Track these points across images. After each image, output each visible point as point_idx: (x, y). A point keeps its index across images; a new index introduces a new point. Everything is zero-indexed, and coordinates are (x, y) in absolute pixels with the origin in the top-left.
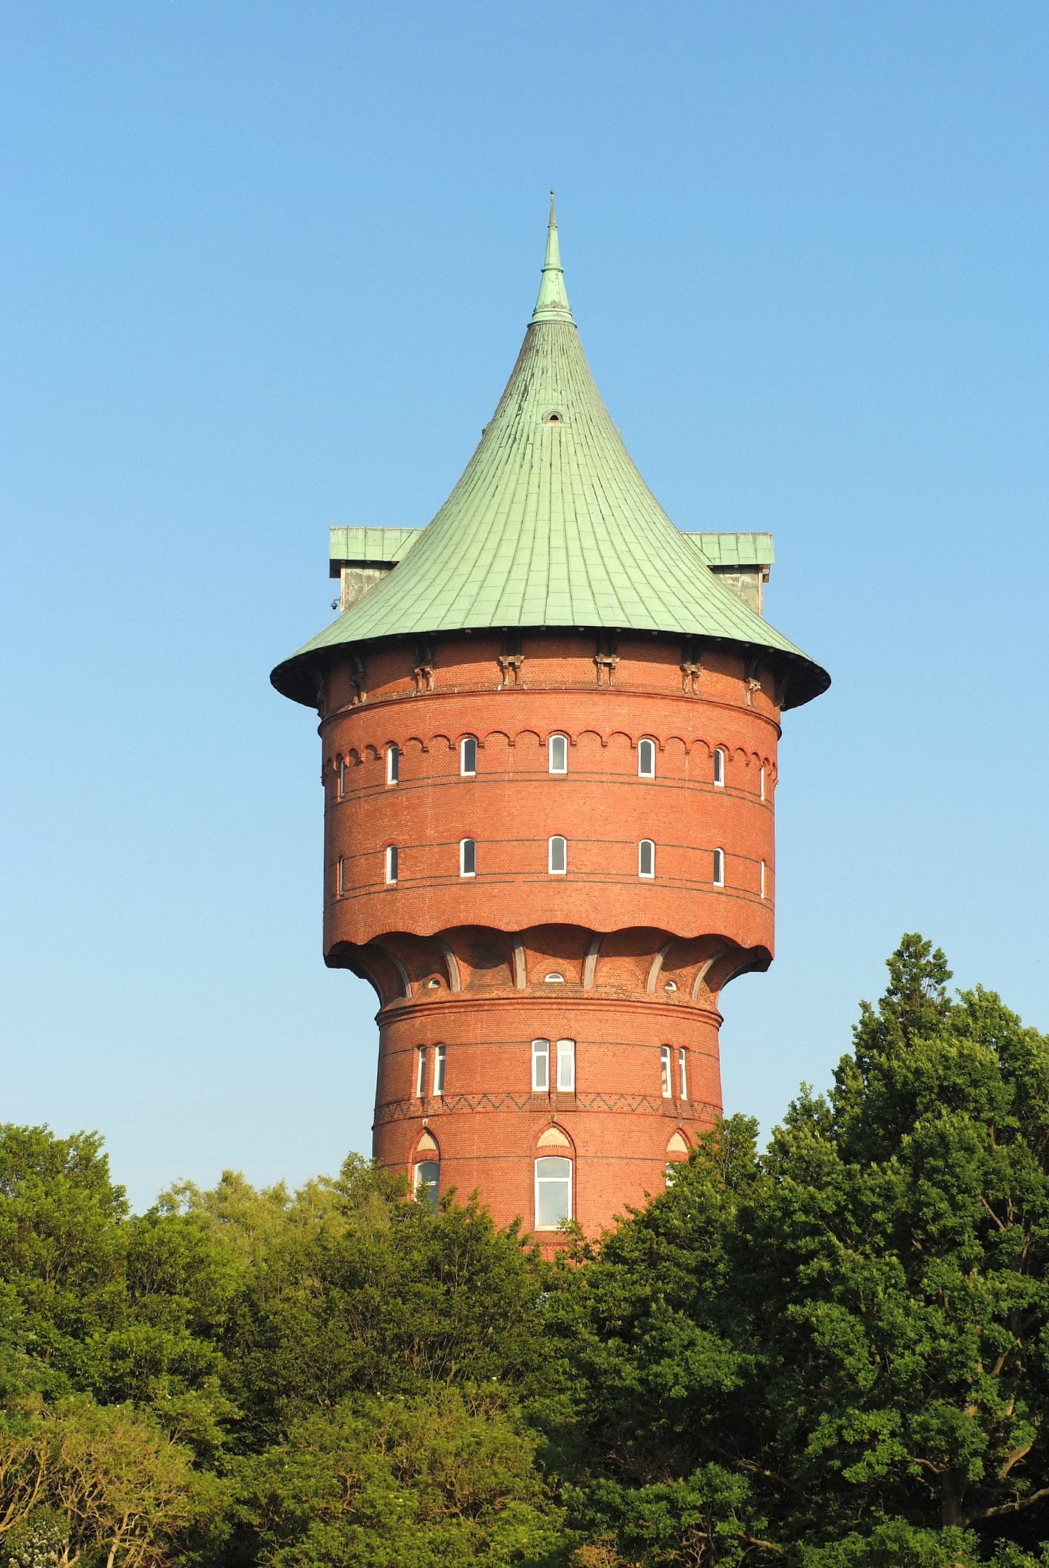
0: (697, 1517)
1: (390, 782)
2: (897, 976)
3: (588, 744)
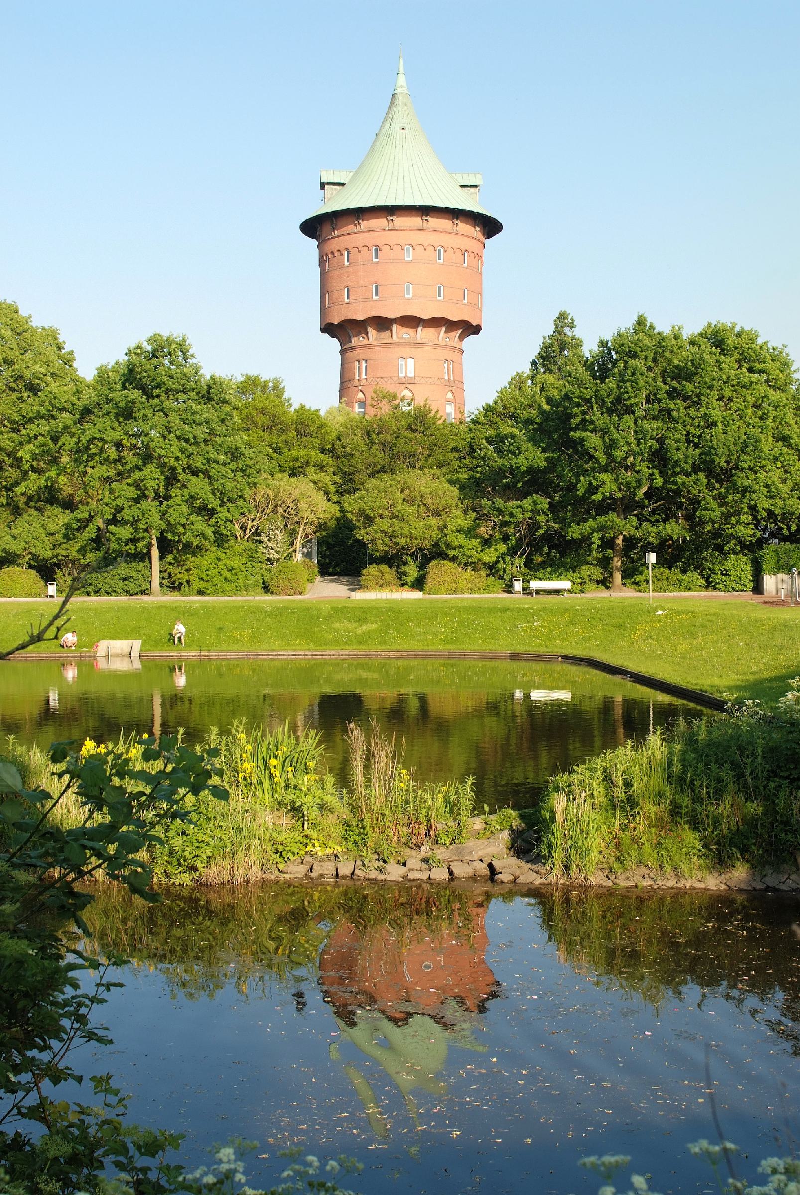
0: (529, 515)
1: (346, 264)
2: (557, 327)
3: (419, 249)
